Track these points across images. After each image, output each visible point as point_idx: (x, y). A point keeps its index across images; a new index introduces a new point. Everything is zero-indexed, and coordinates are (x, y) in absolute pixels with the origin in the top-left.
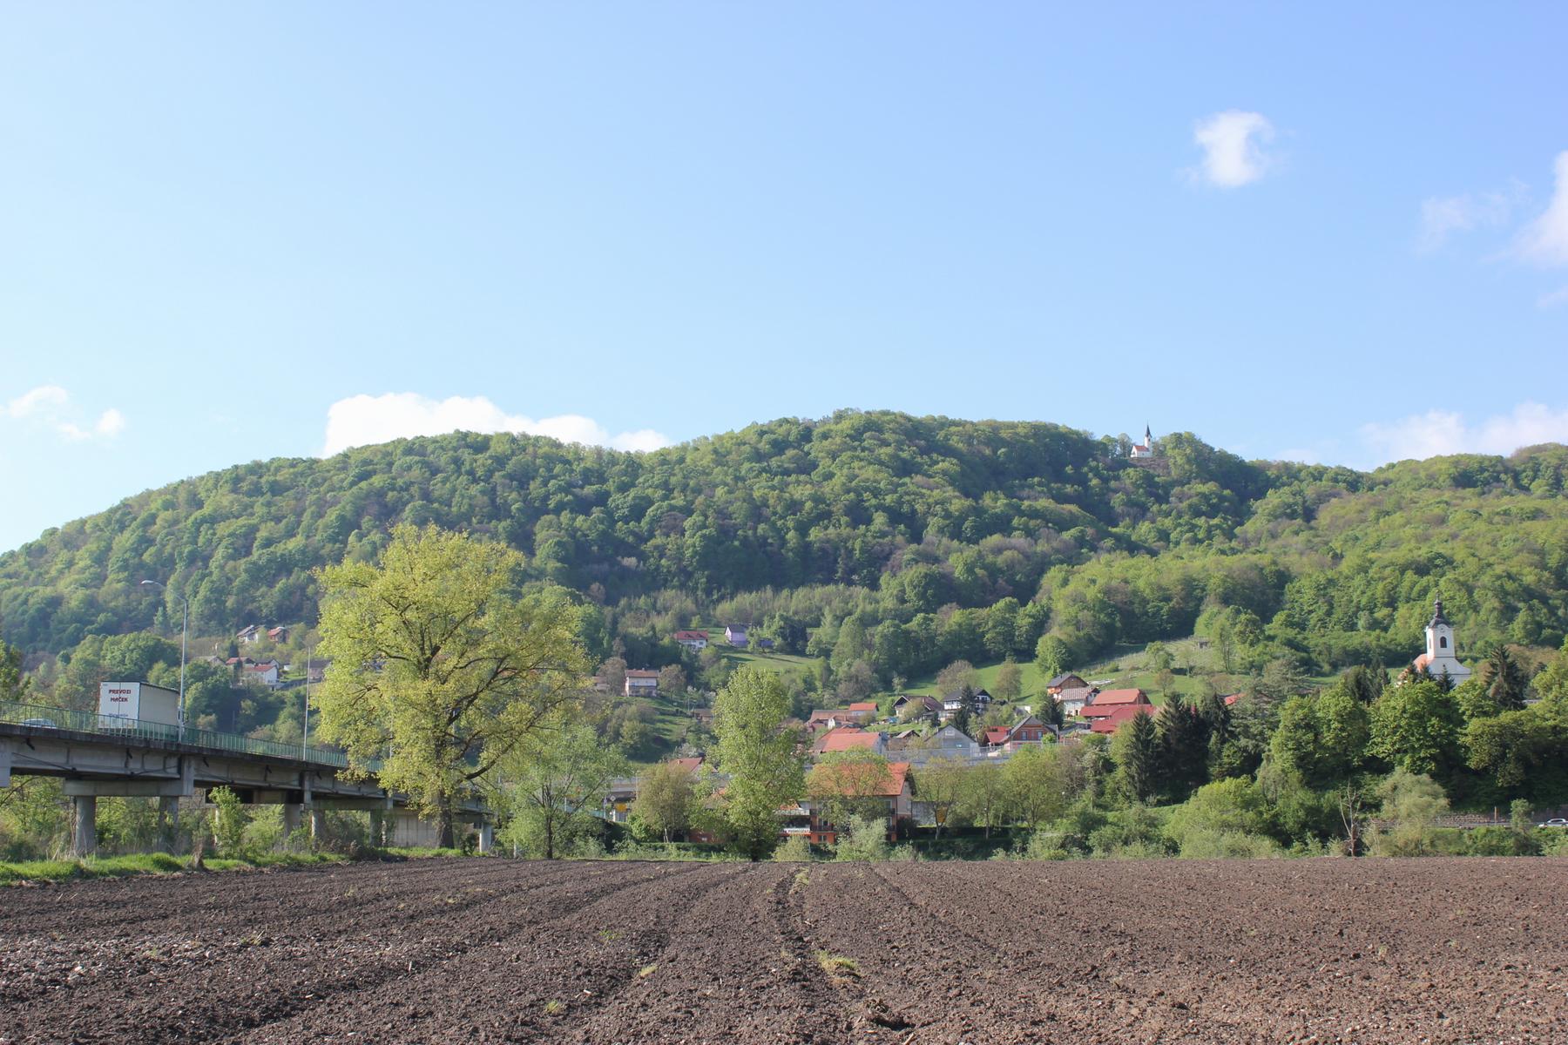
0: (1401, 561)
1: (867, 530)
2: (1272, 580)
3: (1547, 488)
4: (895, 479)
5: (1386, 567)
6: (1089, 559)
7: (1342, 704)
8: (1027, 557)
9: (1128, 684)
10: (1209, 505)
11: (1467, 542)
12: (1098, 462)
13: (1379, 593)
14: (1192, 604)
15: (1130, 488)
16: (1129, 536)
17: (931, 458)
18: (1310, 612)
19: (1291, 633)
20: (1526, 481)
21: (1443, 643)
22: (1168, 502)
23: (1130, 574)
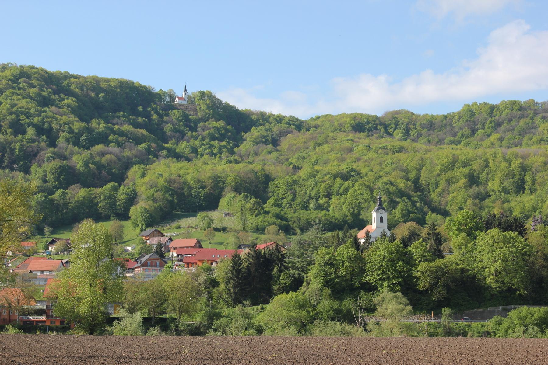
0: (334, 172)
1: (23, 138)
2: (262, 179)
3: (402, 135)
4: (40, 108)
5: (326, 175)
6: (154, 162)
7: (350, 253)
8: (119, 159)
9: (188, 236)
10: (220, 134)
11: (366, 163)
12: (157, 105)
13: (321, 190)
14: (217, 191)
15: (176, 122)
16: (175, 149)
17: (60, 97)
18: (283, 198)
19: (278, 210)
20: (391, 130)
21: (381, 220)
22: (196, 131)
23: (182, 172)
